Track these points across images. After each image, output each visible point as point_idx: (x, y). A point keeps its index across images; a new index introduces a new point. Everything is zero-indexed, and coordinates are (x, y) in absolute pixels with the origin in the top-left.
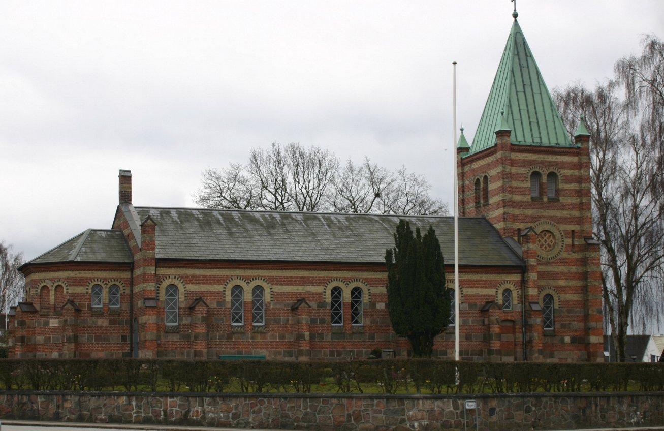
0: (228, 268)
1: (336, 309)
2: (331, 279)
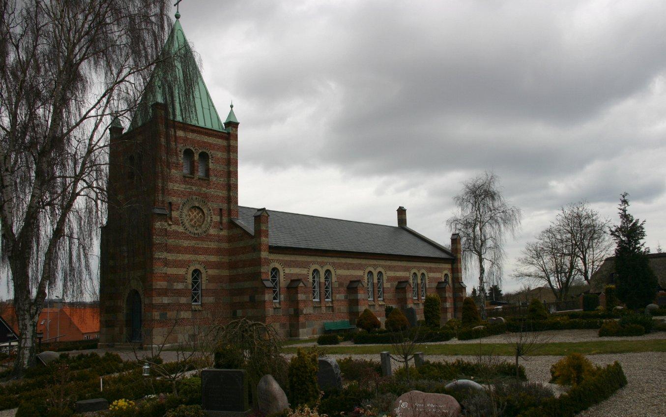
0: (406, 261)
1: (195, 289)
2: (326, 264)
